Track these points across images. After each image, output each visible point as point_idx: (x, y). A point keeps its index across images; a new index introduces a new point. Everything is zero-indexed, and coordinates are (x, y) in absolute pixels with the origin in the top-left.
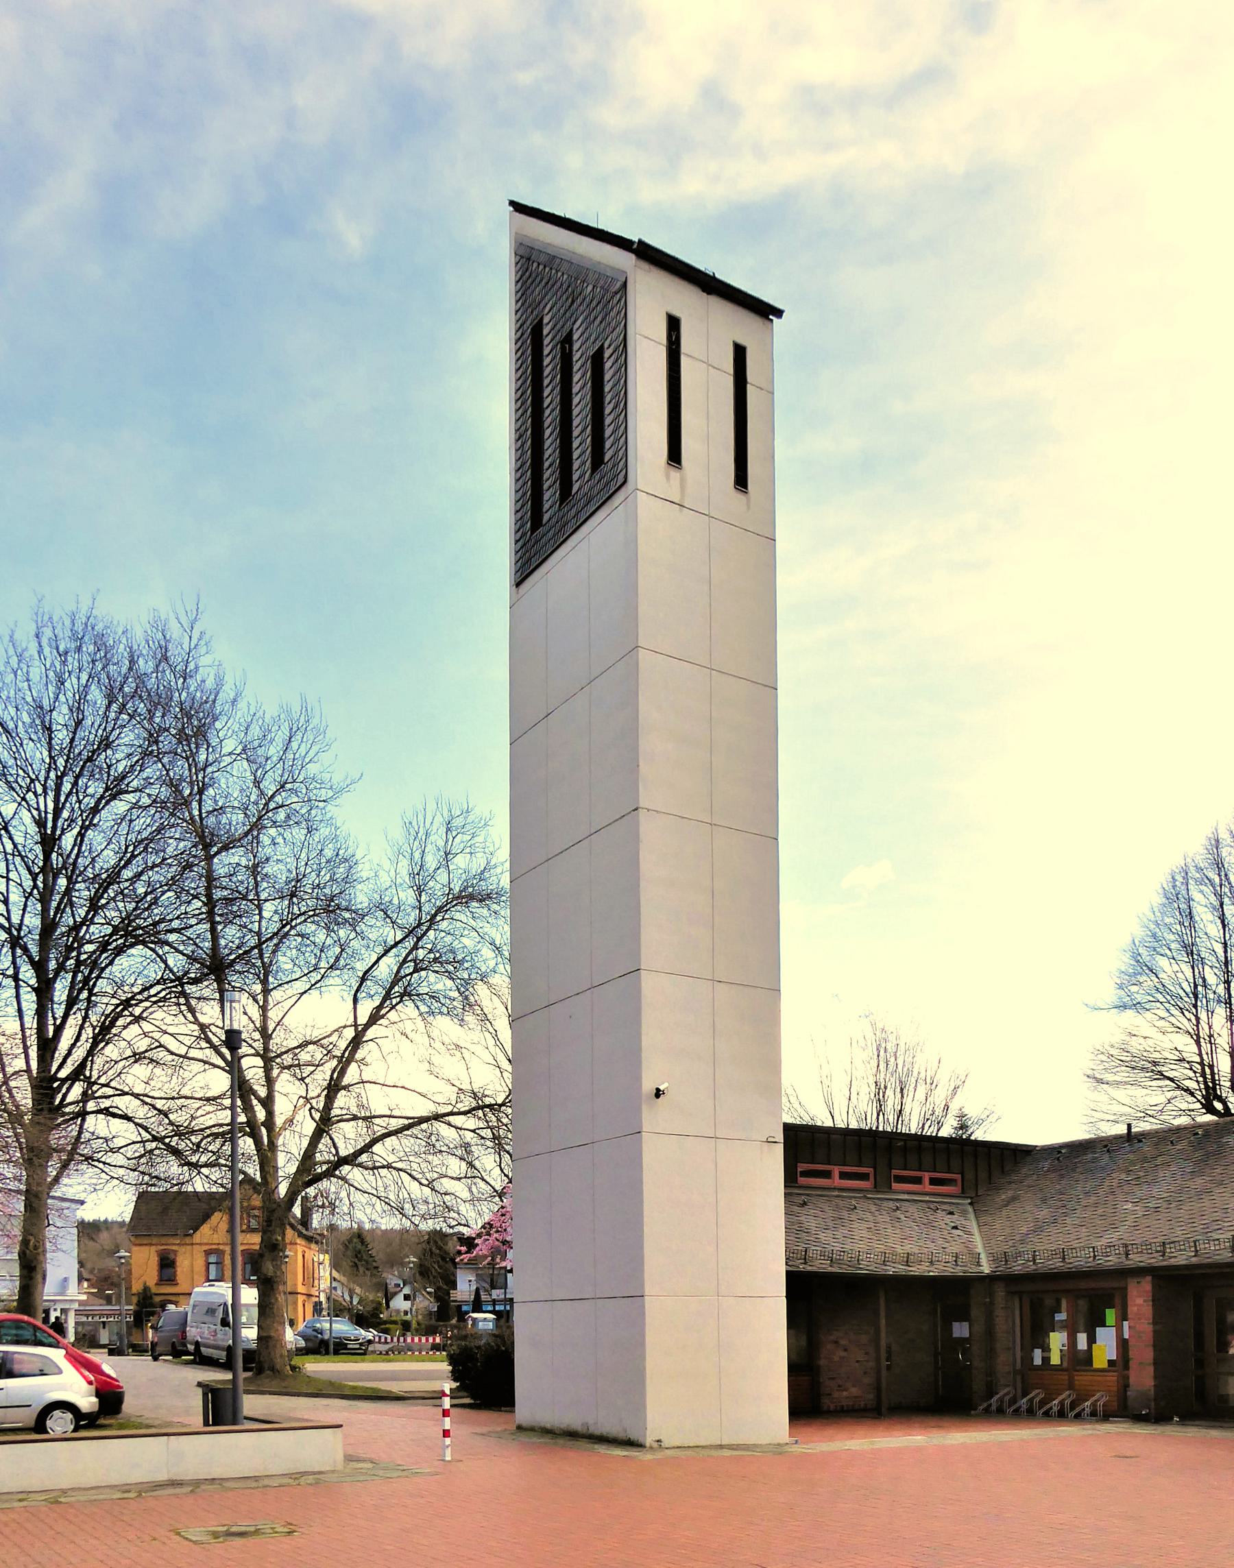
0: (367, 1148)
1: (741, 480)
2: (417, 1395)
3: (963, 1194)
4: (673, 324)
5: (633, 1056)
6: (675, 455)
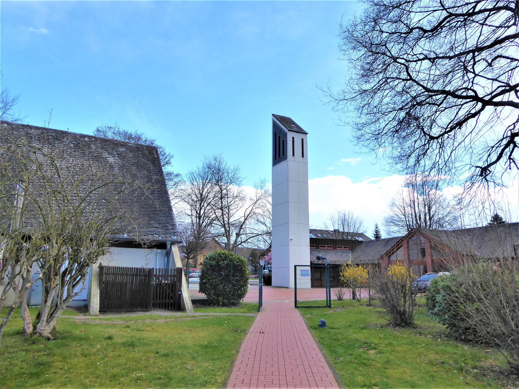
0: (247, 240)
1: (303, 156)
2: (55, 312)
3: (350, 250)
4: (293, 138)
5: (288, 235)
6: (293, 155)
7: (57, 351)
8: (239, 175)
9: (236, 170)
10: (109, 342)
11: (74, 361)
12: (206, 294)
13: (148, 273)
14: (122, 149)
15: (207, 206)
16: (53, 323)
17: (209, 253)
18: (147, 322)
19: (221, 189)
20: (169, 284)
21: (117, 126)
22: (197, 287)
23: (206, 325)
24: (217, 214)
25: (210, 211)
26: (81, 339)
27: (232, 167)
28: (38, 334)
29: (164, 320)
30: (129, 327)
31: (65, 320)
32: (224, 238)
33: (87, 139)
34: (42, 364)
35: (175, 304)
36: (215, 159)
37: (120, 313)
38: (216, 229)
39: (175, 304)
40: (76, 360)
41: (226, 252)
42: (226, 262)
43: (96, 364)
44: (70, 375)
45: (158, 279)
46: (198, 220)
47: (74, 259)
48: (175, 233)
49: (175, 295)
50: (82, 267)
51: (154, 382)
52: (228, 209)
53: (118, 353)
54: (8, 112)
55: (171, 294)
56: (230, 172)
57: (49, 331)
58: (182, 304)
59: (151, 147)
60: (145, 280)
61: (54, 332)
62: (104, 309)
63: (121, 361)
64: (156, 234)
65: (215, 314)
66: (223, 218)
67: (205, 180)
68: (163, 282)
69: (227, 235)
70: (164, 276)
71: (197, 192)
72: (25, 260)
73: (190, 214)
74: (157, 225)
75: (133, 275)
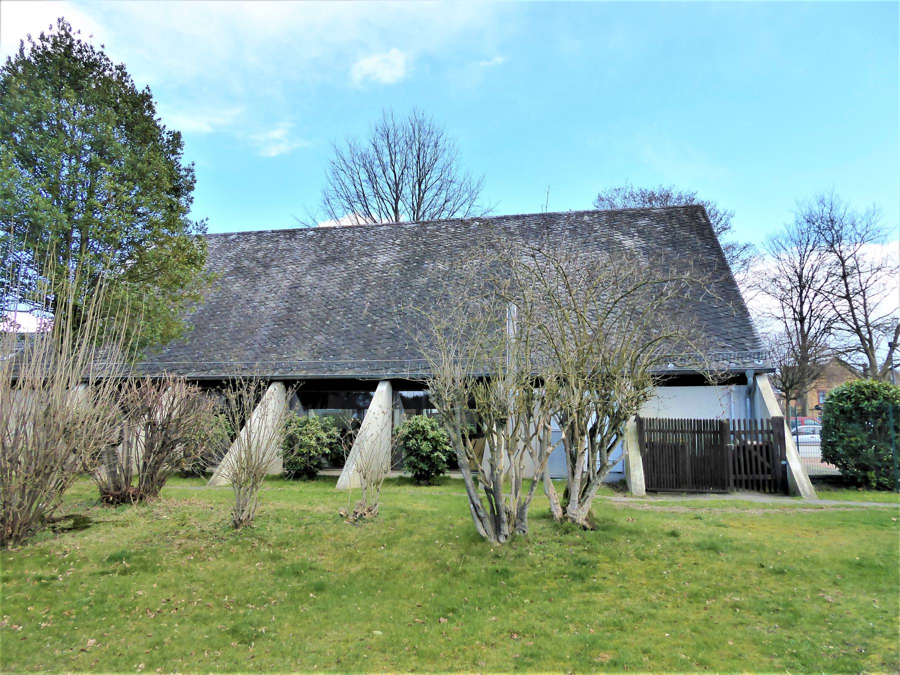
7: (601, 547)
8: (879, 225)
9: (873, 213)
10: (673, 539)
11: (627, 564)
12: (837, 465)
13: (720, 429)
14: (643, 222)
15: (816, 295)
16: (588, 505)
17: (836, 387)
18: (730, 511)
19: (841, 258)
20: (761, 447)
21: (628, 184)
22: (816, 452)
23: (850, 524)
24: (838, 309)
25: (823, 304)
26: (631, 532)
27: (862, 211)
28: (569, 520)
29: (760, 510)
30: (700, 518)
31: (601, 501)
32: (860, 354)
33: (586, 218)
34: (584, 564)
35: (780, 484)
36: (822, 202)
37: (680, 495)
38: (842, 338)
39: (780, 484)
40: (629, 563)
41: (869, 381)
42: (874, 402)
43: (661, 574)
44: (626, 585)
45: (740, 438)
46: (799, 326)
47: (605, 410)
48: (759, 353)
49: (774, 466)
50: (617, 419)
51: (765, 614)
52: (864, 296)
53: (692, 560)
54: (475, 204)
55: (767, 465)
56: (858, 220)
57: (584, 517)
58: (790, 482)
59: (692, 207)
60: (716, 439)
61: (590, 517)
62: (653, 487)
63: (700, 573)
64: (724, 359)
65: (866, 505)
66: (854, 315)
67: (802, 243)
68: (749, 442)
69: (868, 348)
70: (750, 432)
71: (790, 272)
72: (541, 413)
73: (781, 315)
74: (723, 344)
75: (694, 432)
